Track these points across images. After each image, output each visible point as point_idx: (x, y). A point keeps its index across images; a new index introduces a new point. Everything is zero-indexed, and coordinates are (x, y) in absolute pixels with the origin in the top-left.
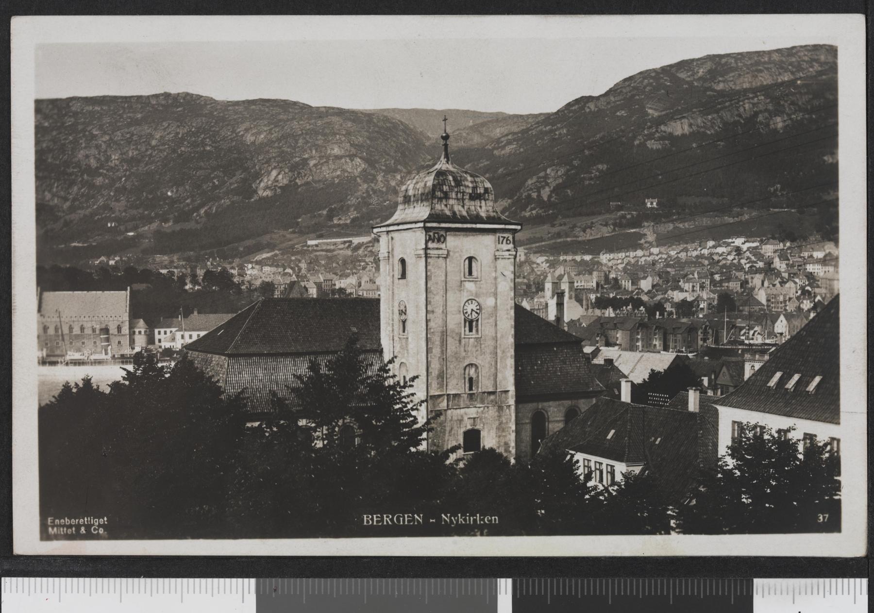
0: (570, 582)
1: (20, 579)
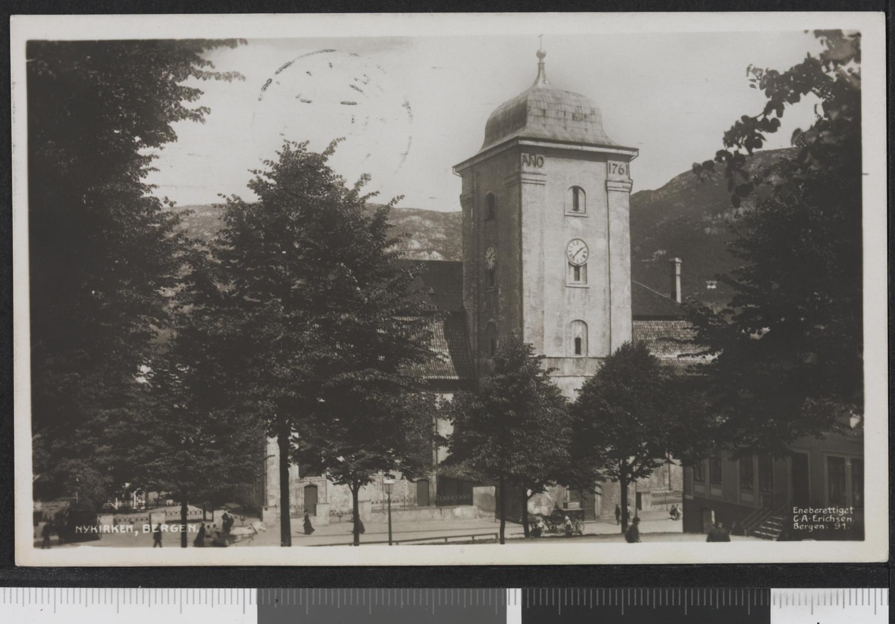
0: (581, 591)
1: (14, 589)
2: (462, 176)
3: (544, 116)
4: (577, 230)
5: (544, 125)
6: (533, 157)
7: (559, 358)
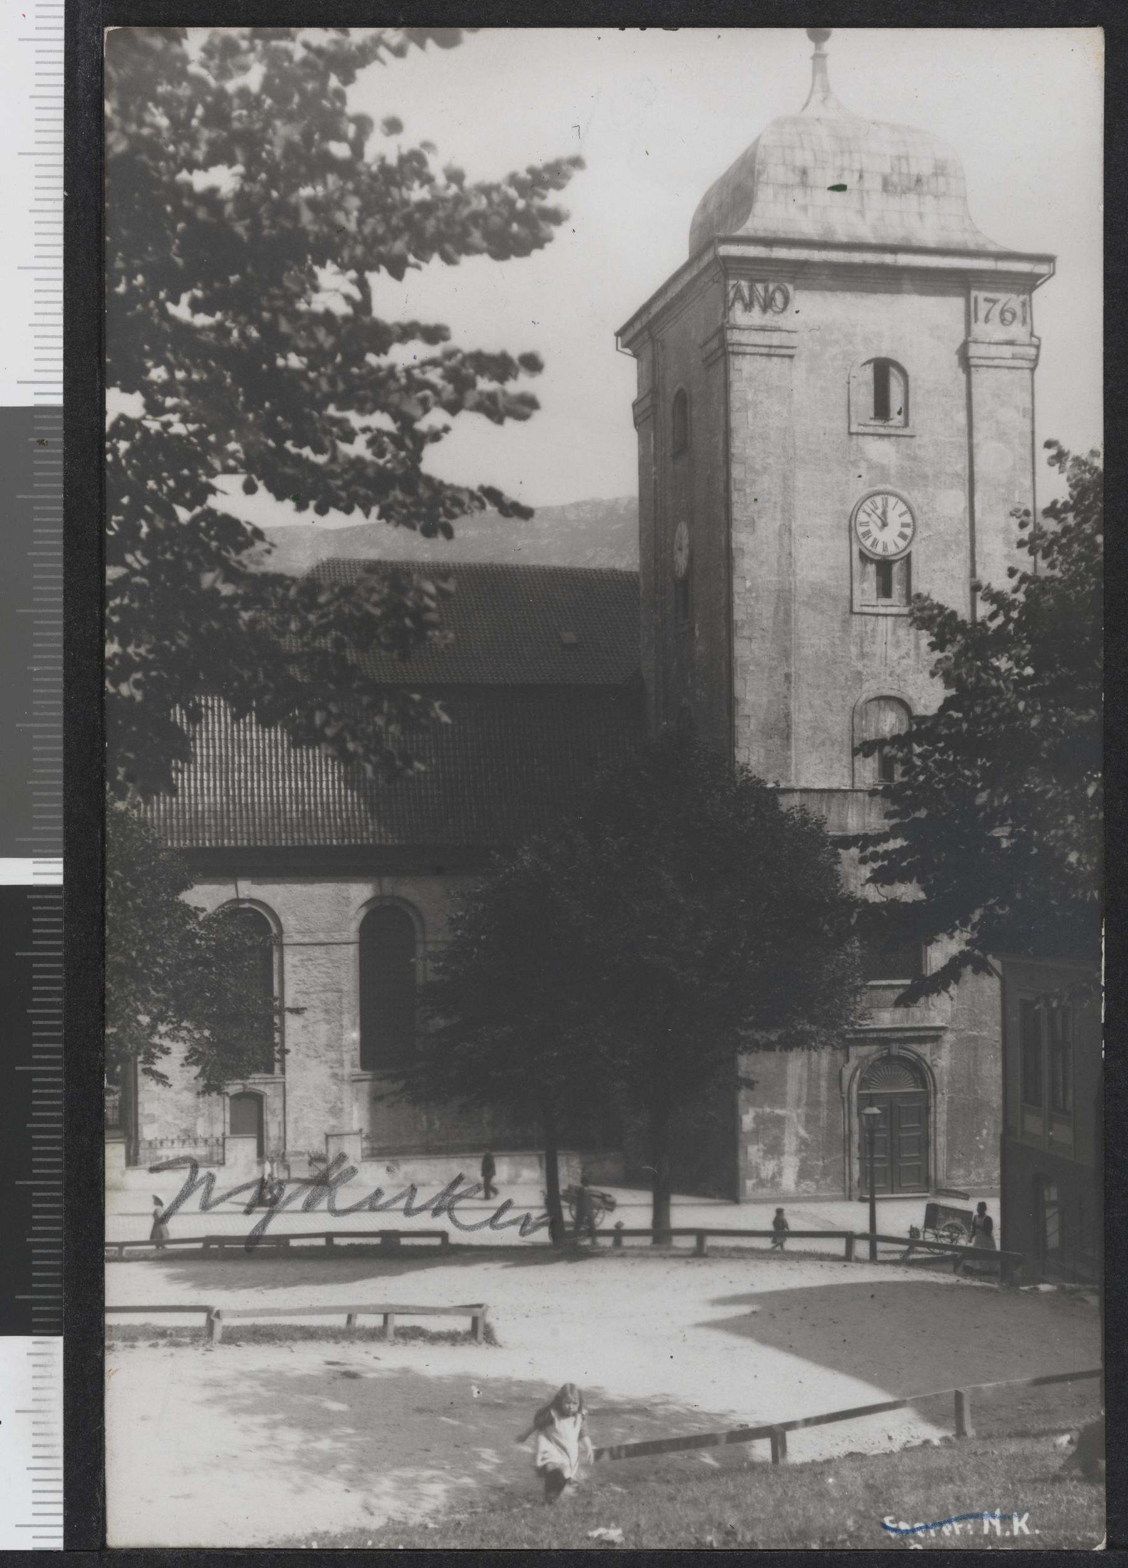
2: (636, 355)
3: (804, 184)
4: (883, 468)
5: (805, 208)
6: (760, 287)
7: (831, 791)
